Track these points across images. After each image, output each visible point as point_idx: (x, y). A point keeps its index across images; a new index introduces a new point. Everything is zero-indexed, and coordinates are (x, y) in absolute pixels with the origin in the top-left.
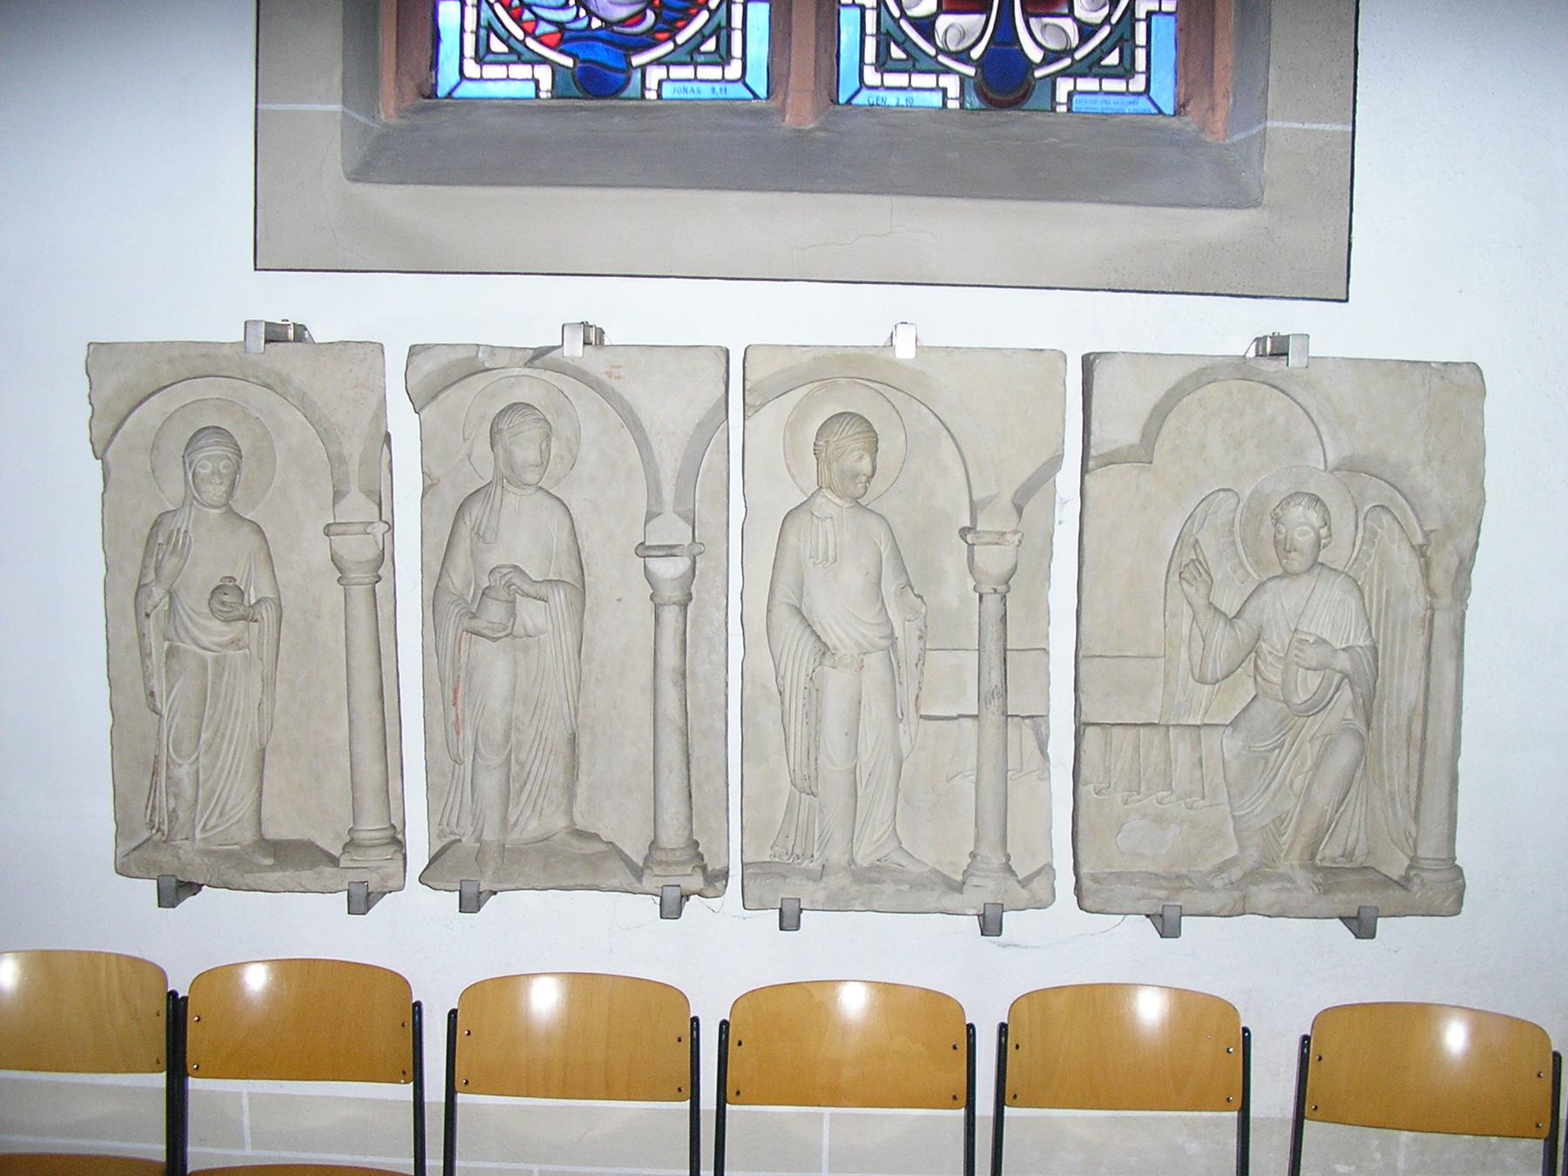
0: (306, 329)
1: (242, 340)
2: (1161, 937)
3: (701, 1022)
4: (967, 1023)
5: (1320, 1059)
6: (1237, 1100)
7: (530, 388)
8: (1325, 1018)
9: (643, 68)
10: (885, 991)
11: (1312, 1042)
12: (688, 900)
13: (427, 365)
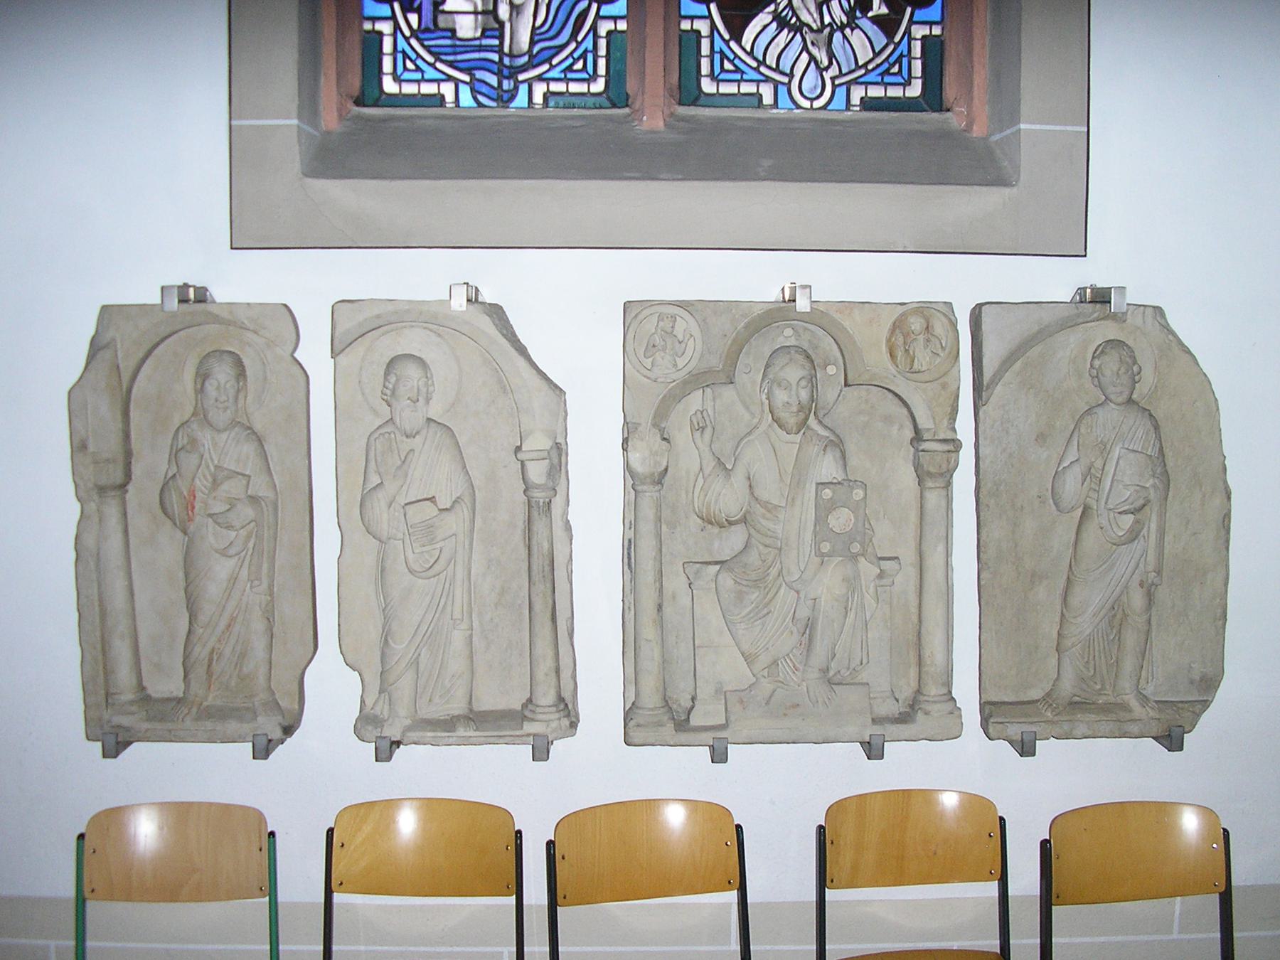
0: (207, 290)
1: (159, 302)
2: (868, 758)
3: (523, 834)
4: (736, 823)
5: (343, 845)
6: (997, 870)
7: (412, 341)
8: (835, 810)
9: (529, 82)
10: (693, 806)
11: (827, 830)
12: (398, 747)
13: (348, 323)
